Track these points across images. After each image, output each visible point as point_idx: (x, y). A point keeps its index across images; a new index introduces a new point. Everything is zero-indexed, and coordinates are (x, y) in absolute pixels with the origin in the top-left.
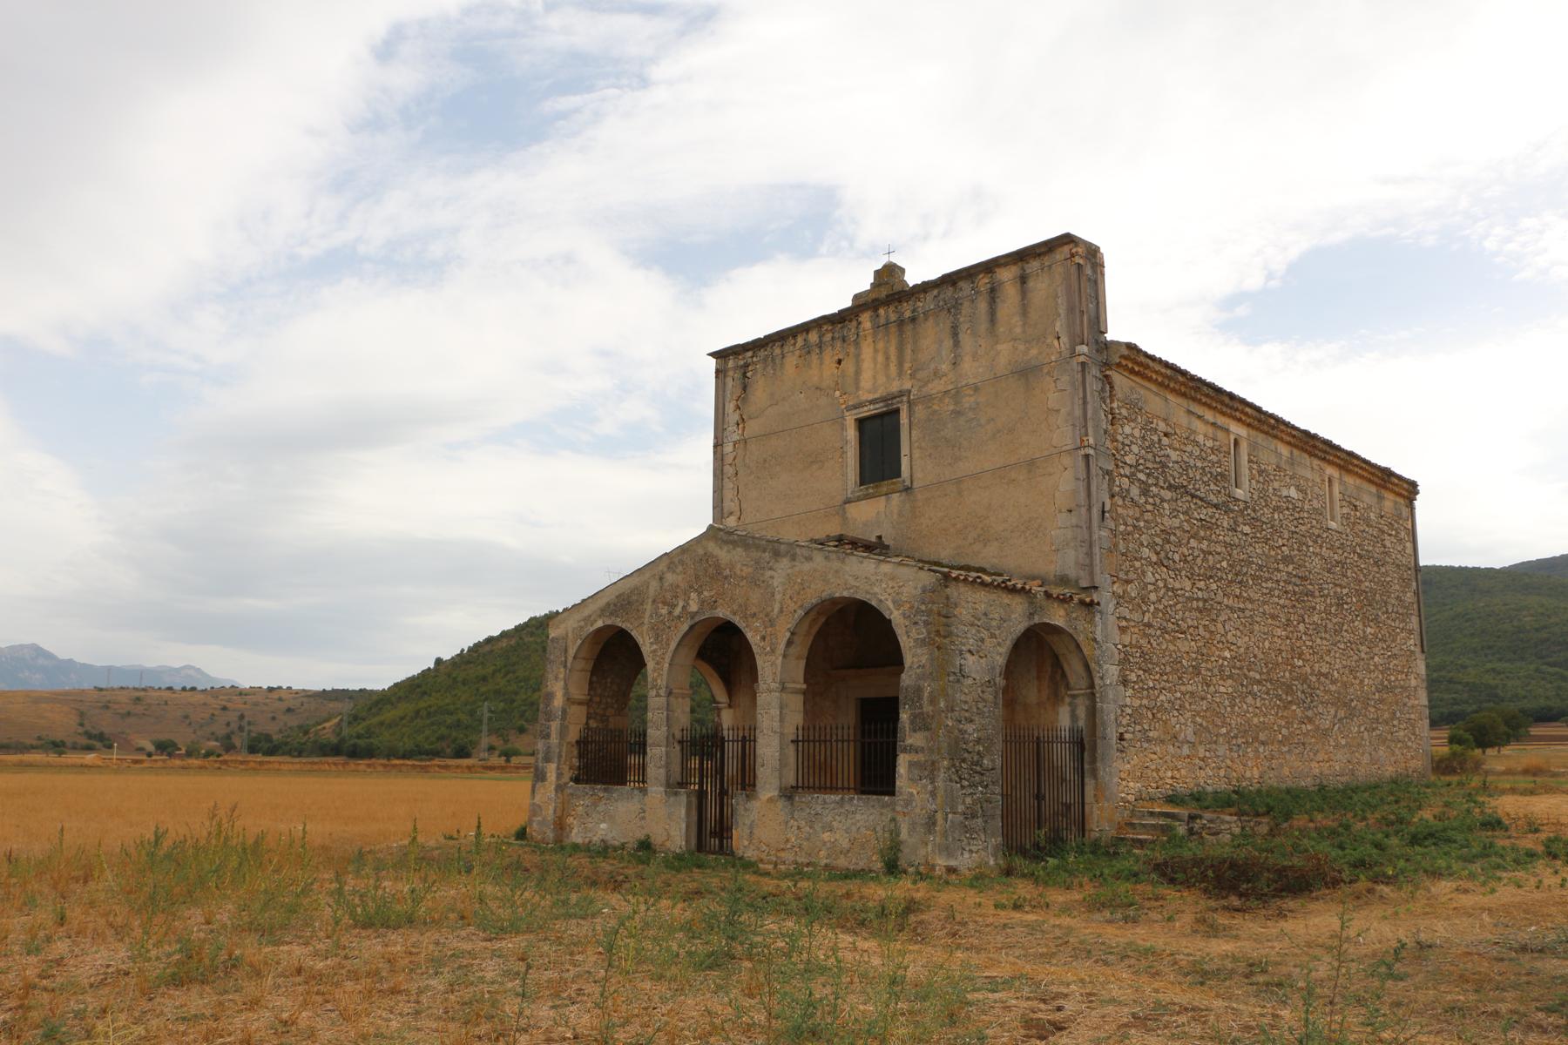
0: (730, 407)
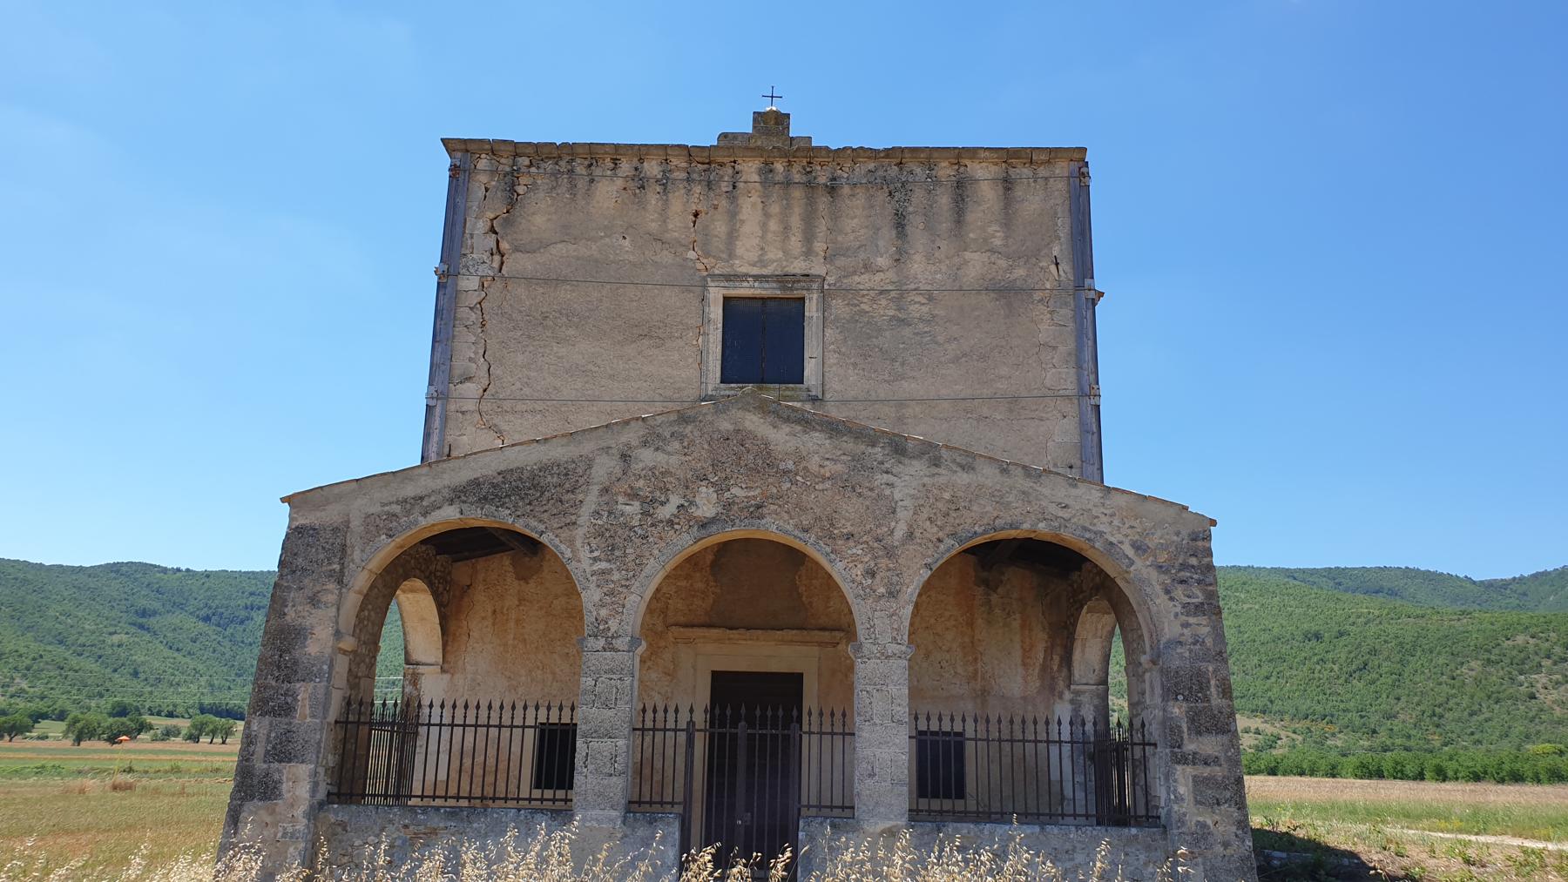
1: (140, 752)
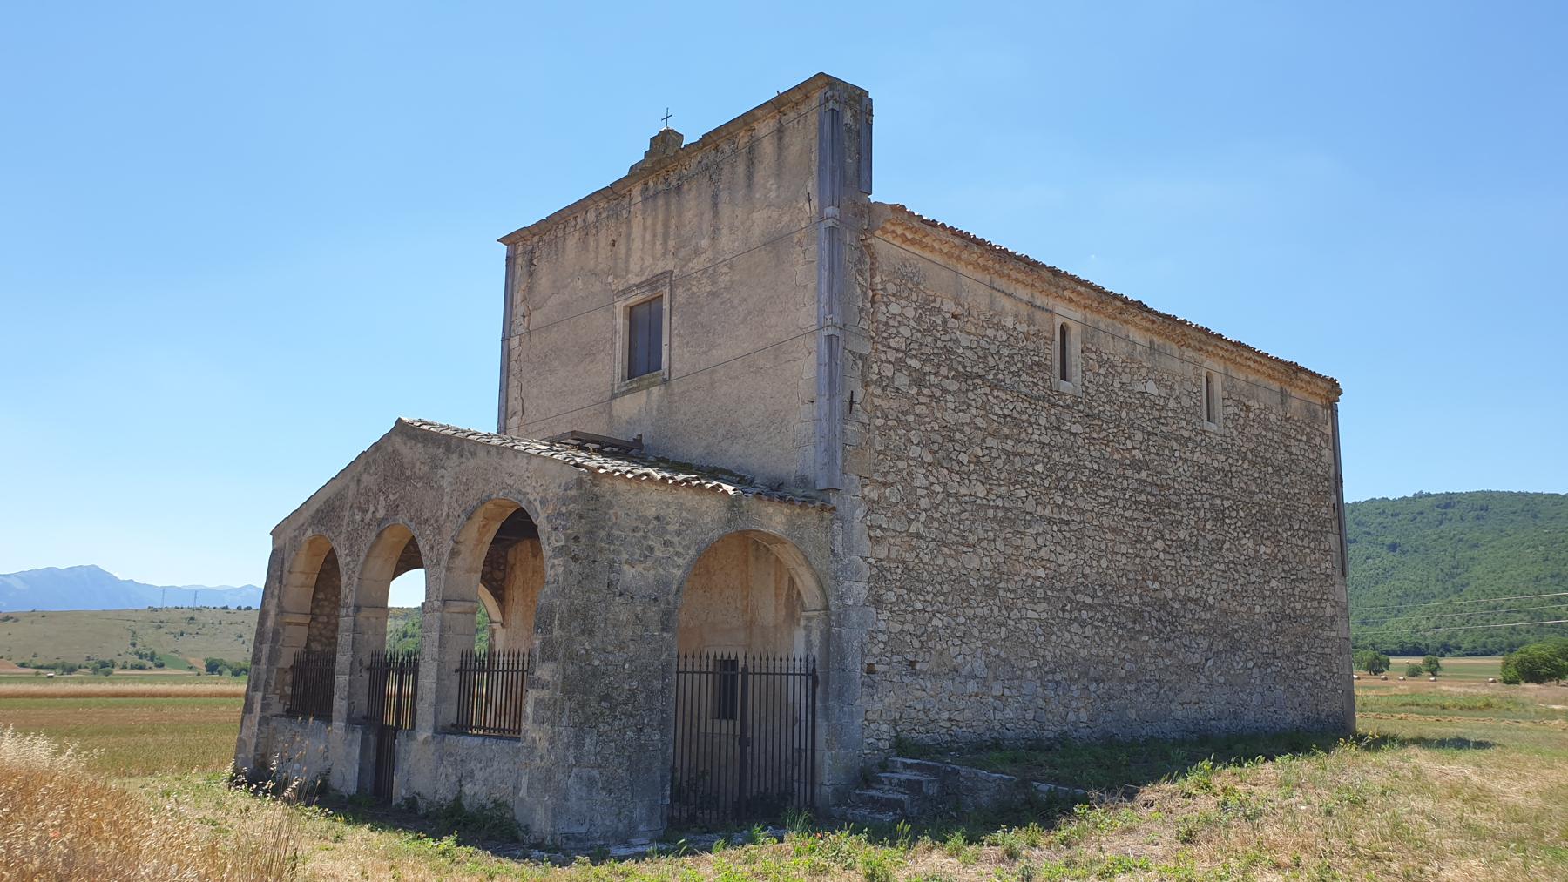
0: (518, 297)
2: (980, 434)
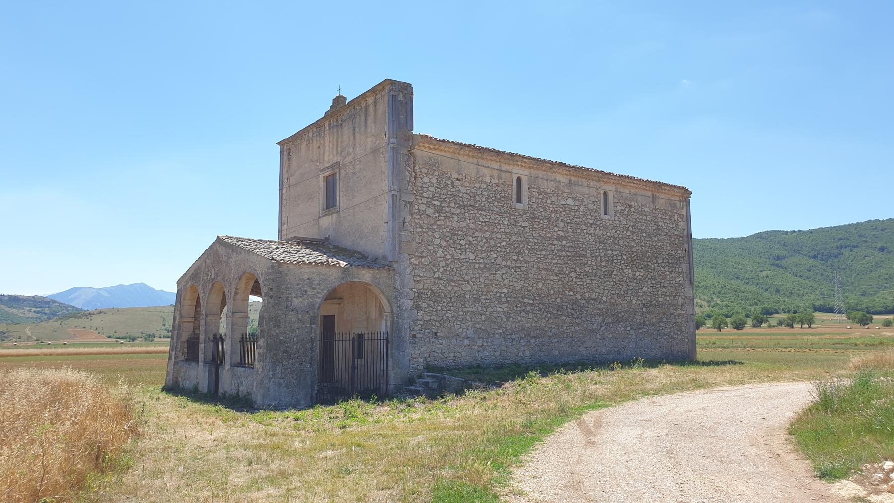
0: (285, 170)
1: (761, 334)
2: (472, 231)
